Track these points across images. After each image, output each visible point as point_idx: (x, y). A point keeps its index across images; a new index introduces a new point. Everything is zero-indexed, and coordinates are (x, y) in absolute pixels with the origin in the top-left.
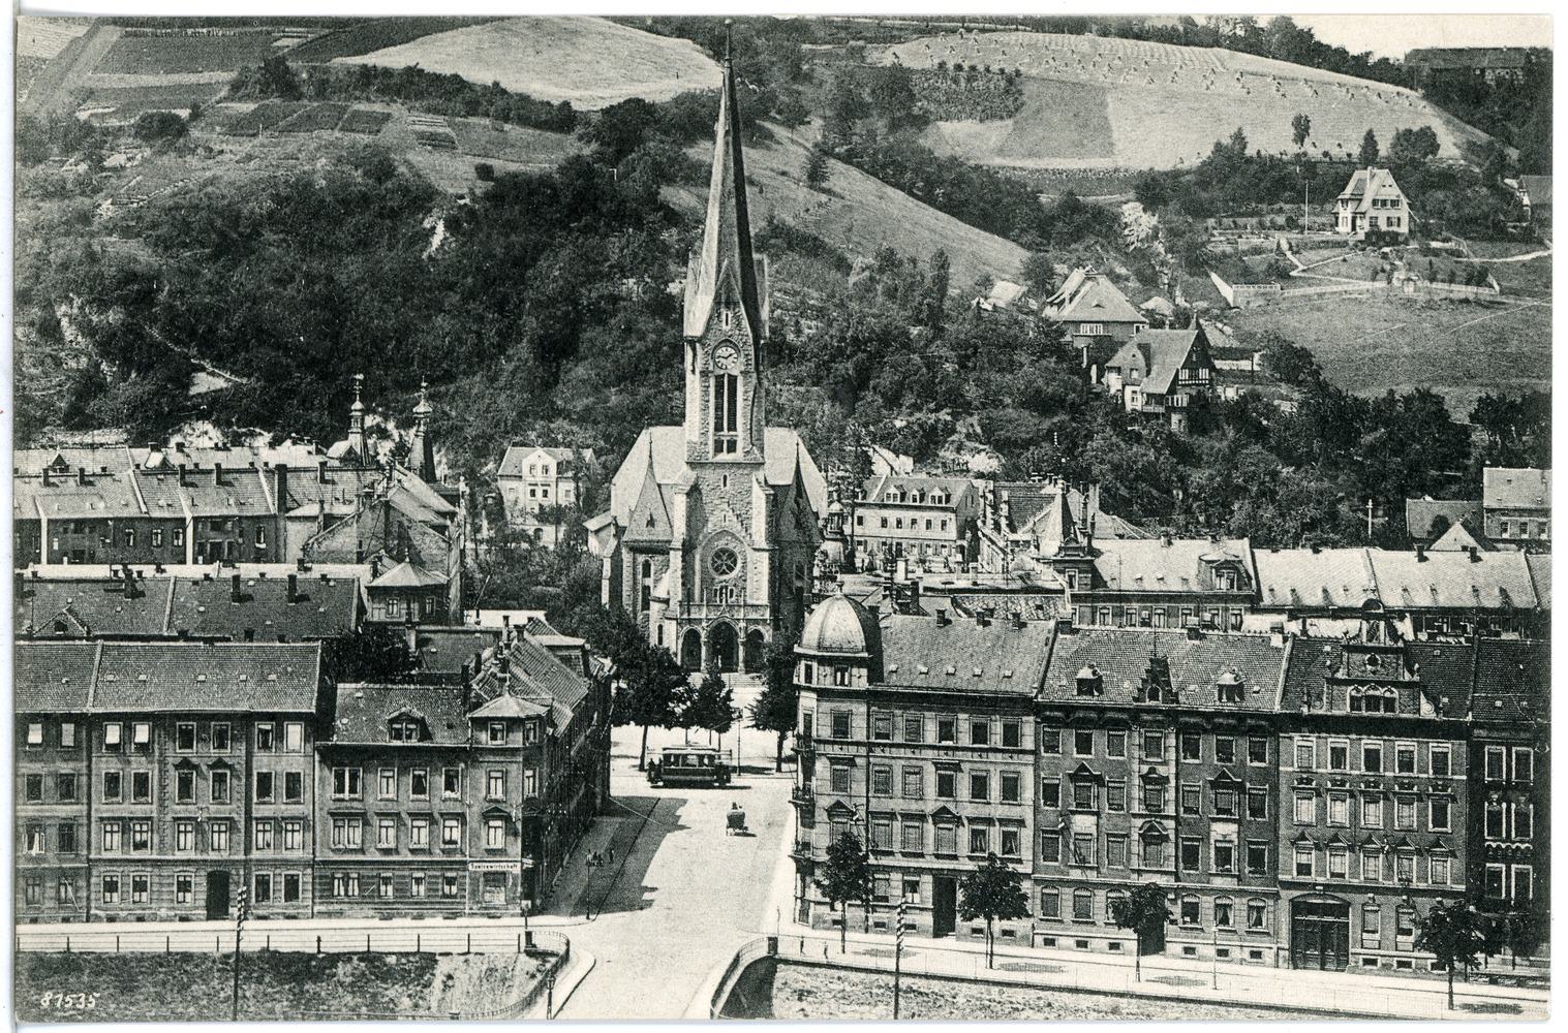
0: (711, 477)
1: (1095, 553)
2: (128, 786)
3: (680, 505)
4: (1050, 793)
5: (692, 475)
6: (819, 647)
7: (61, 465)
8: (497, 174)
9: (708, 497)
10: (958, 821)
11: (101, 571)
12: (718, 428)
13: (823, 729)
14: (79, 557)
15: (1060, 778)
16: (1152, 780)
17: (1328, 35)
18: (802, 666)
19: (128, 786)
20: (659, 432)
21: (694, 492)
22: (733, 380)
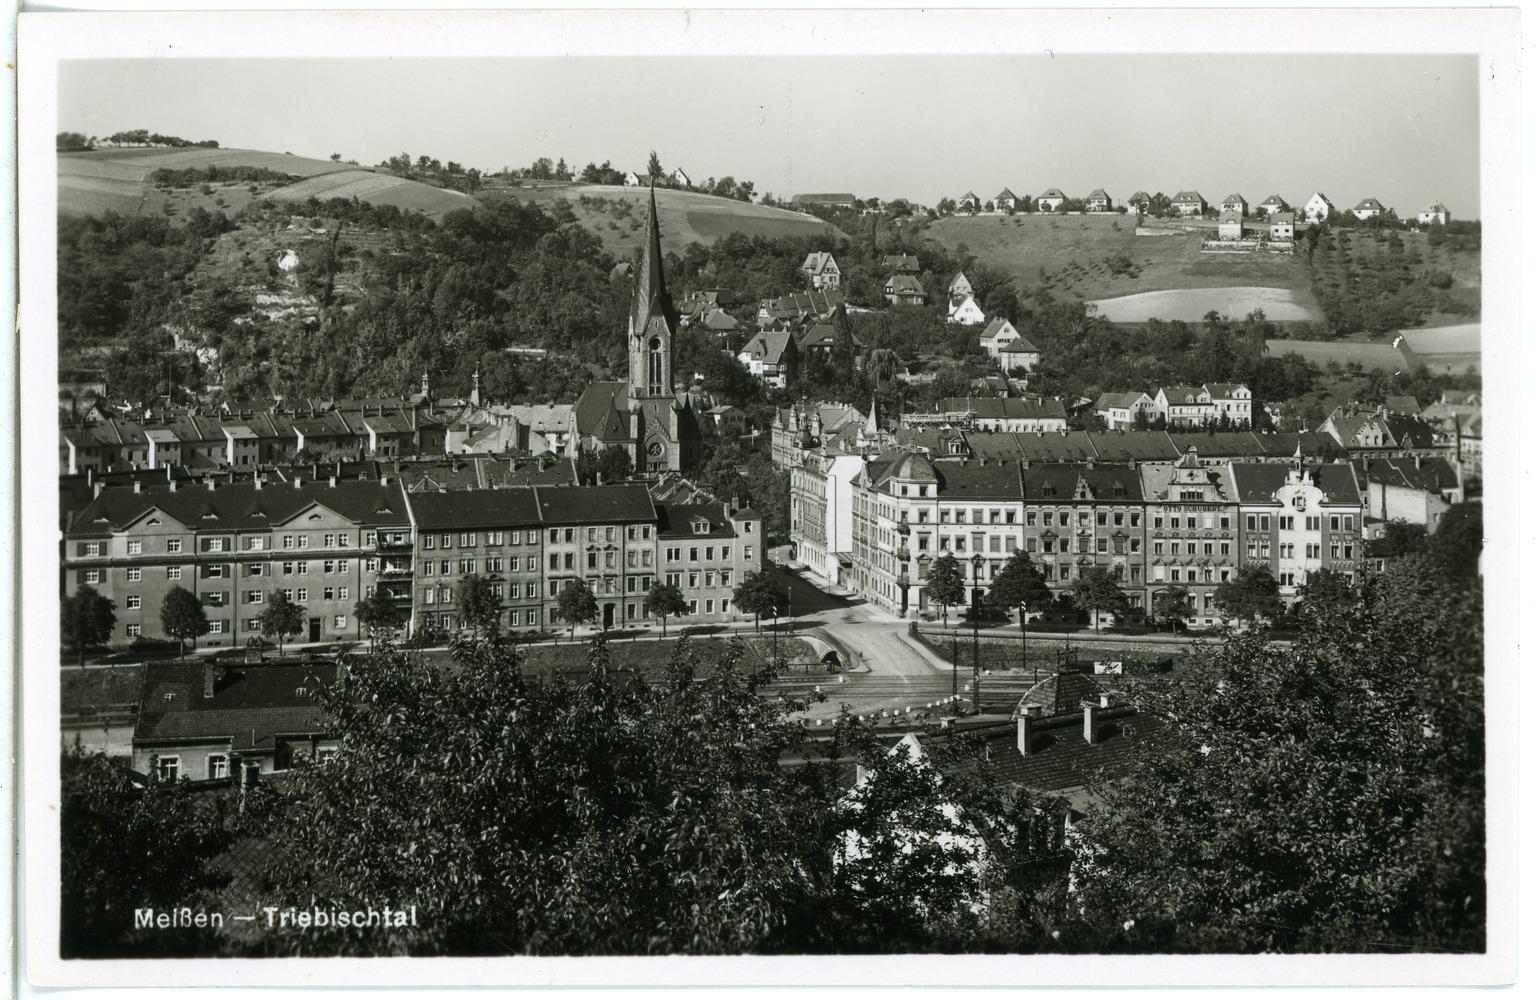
0: (649, 406)
2: (562, 561)
12: (652, 380)
16: (1084, 539)
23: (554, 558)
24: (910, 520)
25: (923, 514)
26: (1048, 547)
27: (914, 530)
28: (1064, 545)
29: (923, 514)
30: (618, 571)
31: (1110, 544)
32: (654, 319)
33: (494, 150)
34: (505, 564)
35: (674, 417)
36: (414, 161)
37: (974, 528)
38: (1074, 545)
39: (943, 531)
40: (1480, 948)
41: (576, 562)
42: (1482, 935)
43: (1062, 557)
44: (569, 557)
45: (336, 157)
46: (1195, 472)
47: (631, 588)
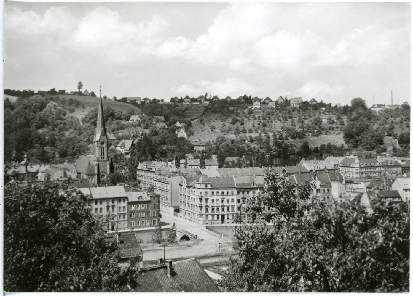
4: (239, 201)
9: (100, 165)
12: (101, 155)
19: (230, 201)
21: (98, 166)
25: (206, 192)
27: (204, 198)
29: (206, 192)
30: (126, 212)
39: (213, 198)
44: (101, 209)
47: (120, 218)
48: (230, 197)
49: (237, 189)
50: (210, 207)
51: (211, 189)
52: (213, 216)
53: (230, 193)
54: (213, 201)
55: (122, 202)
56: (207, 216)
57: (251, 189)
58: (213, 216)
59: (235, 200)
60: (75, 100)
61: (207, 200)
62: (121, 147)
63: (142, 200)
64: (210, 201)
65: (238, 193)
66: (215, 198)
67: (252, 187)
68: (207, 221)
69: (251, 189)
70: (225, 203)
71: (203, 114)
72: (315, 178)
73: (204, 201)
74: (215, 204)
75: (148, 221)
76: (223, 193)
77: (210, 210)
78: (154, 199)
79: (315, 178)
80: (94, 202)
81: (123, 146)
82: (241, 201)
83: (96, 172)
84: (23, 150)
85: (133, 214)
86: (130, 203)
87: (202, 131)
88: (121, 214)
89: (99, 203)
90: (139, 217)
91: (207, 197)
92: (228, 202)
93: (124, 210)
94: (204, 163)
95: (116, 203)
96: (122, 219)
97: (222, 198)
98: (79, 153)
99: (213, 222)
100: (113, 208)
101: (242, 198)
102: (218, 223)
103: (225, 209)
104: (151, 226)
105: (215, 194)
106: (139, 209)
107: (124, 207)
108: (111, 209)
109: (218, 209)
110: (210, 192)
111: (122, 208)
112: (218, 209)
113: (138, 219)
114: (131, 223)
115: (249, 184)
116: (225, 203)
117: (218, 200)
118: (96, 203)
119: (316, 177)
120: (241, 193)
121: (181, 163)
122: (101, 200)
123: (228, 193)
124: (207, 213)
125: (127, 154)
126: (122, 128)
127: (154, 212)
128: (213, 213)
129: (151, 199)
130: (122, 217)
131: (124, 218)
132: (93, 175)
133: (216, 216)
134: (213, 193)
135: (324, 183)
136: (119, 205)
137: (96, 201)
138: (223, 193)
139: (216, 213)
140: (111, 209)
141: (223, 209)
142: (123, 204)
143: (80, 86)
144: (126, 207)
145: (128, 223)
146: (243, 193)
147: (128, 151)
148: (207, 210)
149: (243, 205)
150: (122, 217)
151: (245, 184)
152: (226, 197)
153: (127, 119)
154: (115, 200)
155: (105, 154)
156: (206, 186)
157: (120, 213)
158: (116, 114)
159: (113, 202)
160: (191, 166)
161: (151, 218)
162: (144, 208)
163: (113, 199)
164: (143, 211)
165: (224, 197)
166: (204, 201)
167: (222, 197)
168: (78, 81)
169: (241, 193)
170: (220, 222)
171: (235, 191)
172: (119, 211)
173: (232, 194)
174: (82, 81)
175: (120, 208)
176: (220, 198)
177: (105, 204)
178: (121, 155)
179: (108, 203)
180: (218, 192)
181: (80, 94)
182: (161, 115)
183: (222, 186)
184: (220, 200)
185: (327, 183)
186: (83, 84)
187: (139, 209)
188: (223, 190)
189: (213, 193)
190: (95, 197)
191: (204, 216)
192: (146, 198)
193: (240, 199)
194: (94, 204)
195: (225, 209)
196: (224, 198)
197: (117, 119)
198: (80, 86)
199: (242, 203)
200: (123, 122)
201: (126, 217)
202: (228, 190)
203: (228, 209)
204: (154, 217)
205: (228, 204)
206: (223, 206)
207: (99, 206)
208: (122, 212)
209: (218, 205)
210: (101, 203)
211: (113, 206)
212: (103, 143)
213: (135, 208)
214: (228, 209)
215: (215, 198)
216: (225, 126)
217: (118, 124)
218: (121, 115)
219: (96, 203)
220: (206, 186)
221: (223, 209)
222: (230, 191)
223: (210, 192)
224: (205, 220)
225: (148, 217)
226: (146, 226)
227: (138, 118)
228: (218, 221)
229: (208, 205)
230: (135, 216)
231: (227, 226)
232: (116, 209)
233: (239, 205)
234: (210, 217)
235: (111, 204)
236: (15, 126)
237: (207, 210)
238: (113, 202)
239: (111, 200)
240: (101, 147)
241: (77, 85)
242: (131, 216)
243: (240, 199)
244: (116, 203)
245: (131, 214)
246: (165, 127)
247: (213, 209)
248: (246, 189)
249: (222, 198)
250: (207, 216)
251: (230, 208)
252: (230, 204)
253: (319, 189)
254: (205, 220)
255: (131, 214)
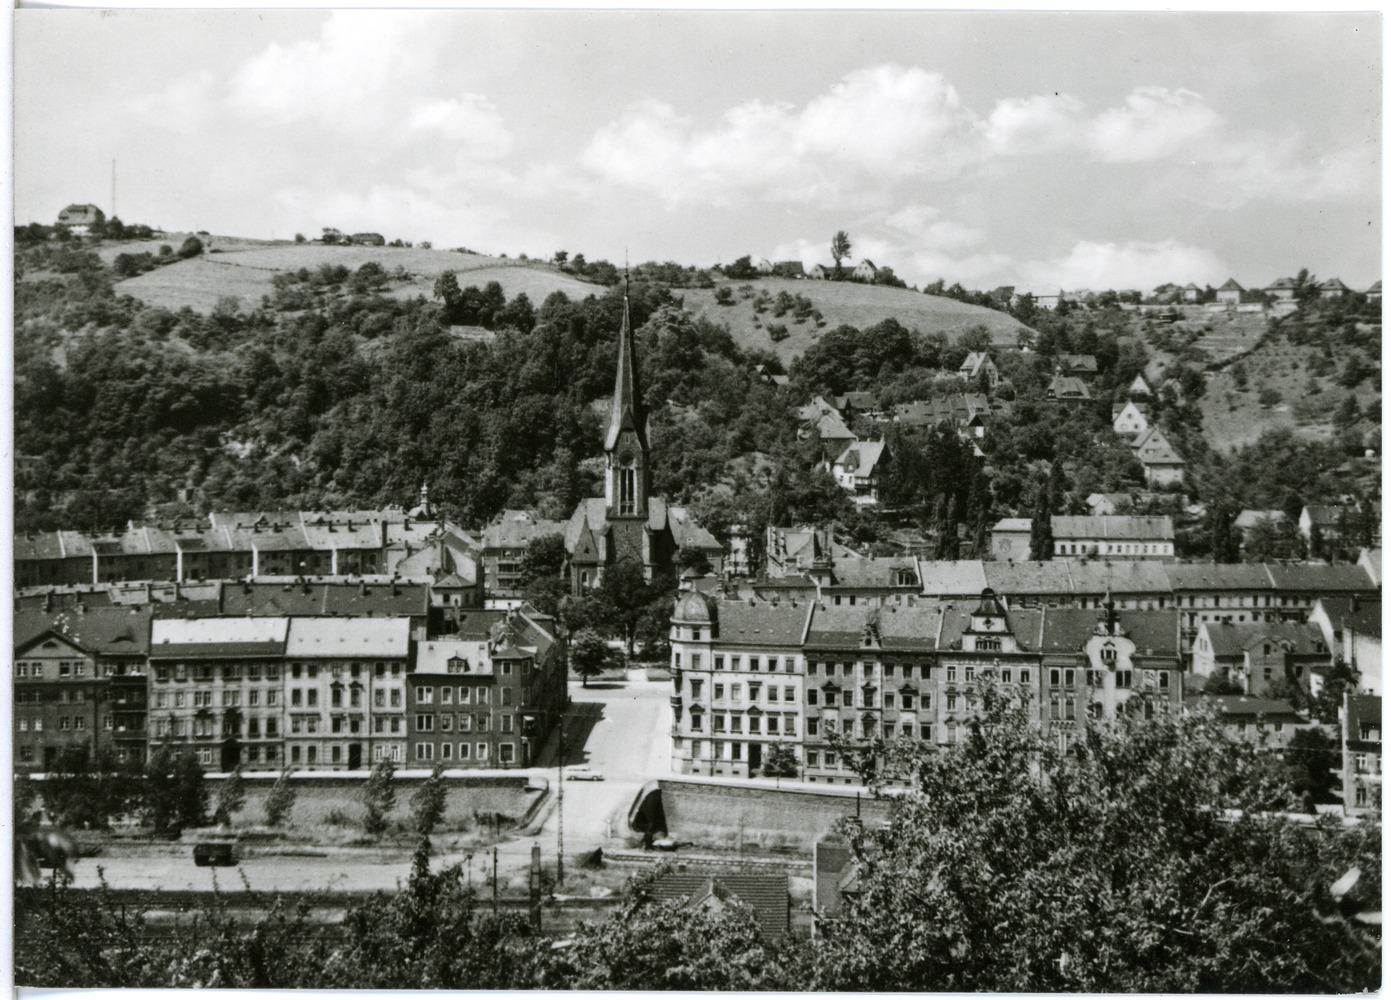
0: (620, 526)
1: (833, 565)
2: (781, 694)
3: (602, 542)
4: (812, 697)
5: (609, 524)
6: (684, 618)
7: (264, 522)
8: (1334, 627)
9: (617, 535)
10: (760, 713)
11: (289, 579)
12: (623, 499)
13: (686, 662)
14: (276, 571)
15: (895, 691)
16: (869, 691)
17: (970, 288)
18: (674, 628)
19: (781, 694)
20: (591, 502)
21: (610, 535)
22: (631, 472)
23: (297, 694)
24: (682, 667)
25: (696, 658)
26: (907, 703)
27: (687, 677)
28: (926, 701)
29: (696, 658)
30: (403, 708)
31: (899, 699)
32: (625, 435)
33: (627, 250)
34: (244, 700)
35: (646, 539)
36: (571, 258)
37: (751, 677)
38: (859, 698)
39: (718, 678)
40: (21, 979)
41: (320, 698)
42: (68, 977)
43: (925, 715)
44: (313, 693)
45: (504, 256)
46: (992, 620)
47: (379, 729)
48: (781, 681)
49: (805, 652)
50: (708, 711)
51: (712, 646)
52: (718, 744)
53: (781, 665)
54: (719, 690)
55: (388, 674)
56: (696, 743)
57: (859, 655)
58: (718, 744)
59: (800, 695)
60: (798, 298)
61: (696, 685)
62: (845, 466)
63: (462, 671)
64: (707, 690)
65: (812, 668)
66: (726, 679)
67: (863, 647)
68: (697, 764)
69: (859, 655)
70: (763, 702)
71: (1259, 346)
72: (1111, 629)
73: (687, 687)
74: (726, 702)
75: (482, 747)
76: (754, 664)
77: (706, 722)
78: (507, 670)
79: (1111, 629)
80: (289, 666)
81: (854, 462)
82: (821, 696)
83: (603, 555)
84: (521, 469)
85: (429, 719)
86: (417, 681)
87: (1233, 409)
88: (385, 715)
89: (305, 675)
90: (450, 729)
91: (699, 676)
92: (773, 697)
93: (394, 703)
94: (1049, 531)
95: (364, 677)
96: (387, 732)
97: (751, 683)
98: (693, 482)
99: (718, 766)
100: (355, 694)
101: (902, 691)
102: (736, 773)
103: (764, 721)
104: (495, 765)
105: (727, 663)
106: (449, 701)
107: (395, 693)
108: (346, 696)
109: (736, 721)
110: (707, 657)
111: (388, 695)
112: (736, 721)
113: (446, 736)
114: (421, 747)
115: (856, 637)
116: (763, 702)
117: (735, 687)
118: (297, 674)
119: (1117, 626)
120: (821, 668)
121: (1055, 533)
122: (315, 664)
123: (772, 664)
124: (696, 735)
125: (862, 490)
126: (922, 395)
127: (507, 718)
128: (719, 735)
129: (494, 670)
130: (387, 725)
131: (395, 729)
132: (594, 565)
133: (728, 749)
134: (719, 662)
135: (1149, 652)
136: (377, 684)
137: (298, 665)
138: (754, 664)
139: (728, 735)
140: (346, 696)
141: (754, 725)
142: (391, 682)
143: (842, 245)
144: (403, 693)
145: (411, 746)
146: (830, 670)
147: (866, 482)
148: (696, 722)
149: (830, 714)
150: (387, 725)
151: (845, 634)
152: (768, 680)
153: (955, 363)
154: (363, 666)
155: (635, 494)
156: (697, 636)
157: (381, 710)
158: (920, 346)
159: (356, 672)
160: (1073, 539)
161: (493, 738)
162: (467, 701)
163: (356, 663)
164: (464, 710)
165: (758, 678)
166: (687, 687)
167: (751, 677)
168: (835, 234)
169: (821, 668)
170: (744, 767)
171: (800, 661)
172: (378, 704)
173: (790, 670)
174: (845, 229)
175: (380, 693)
176: (743, 680)
177: (323, 681)
178: (842, 493)
179: (336, 676)
180: (736, 660)
181: (840, 274)
182: (1088, 352)
183: (754, 639)
184: (745, 690)
185: (1165, 653)
186: (850, 239)
187: (449, 701)
188: (755, 654)
189: (719, 662)
190: (294, 650)
191: (687, 744)
192: (481, 665)
193: (818, 689)
194: (289, 675)
195: (764, 721)
196: (759, 683)
197: (920, 362)
198: (842, 245)
199: (824, 704)
200: (940, 376)
201: (403, 725)
202: (772, 655)
203: (773, 725)
204: (507, 732)
205: (772, 707)
206: (753, 711)
207: (305, 683)
208: (388, 708)
209: (735, 708)
210: (313, 673)
211: (356, 687)
212: (626, 459)
213: (436, 698)
214: (773, 725)
215: (726, 679)
216: (1317, 391)
217: (911, 380)
218: (940, 350)
219: (297, 674)
220: (697, 636)
221: (754, 725)
222: (781, 659)
223: (707, 657)
224: (689, 756)
225: (481, 732)
226: (474, 764)
227: (985, 361)
228: (737, 766)
229: (701, 704)
230: (436, 728)
231: (729, 788)
232: (364, 697)
233: (812, 711)
234: (707, 750)
235: (347, 678)
236: (512, 388)
237: (696, 722)
238: (356, 672)
239: (347, 666)
240: (623, 473)
241: (829, 245)
242: (421, 726)
243: (818, 689)
244: (364, 677)
245: (421, 719)
246: (1080, 394)
247: (719, 722)
248: (840, 653)
249: (751, 683)
250: (696, 743)
251: (781, 721)
252: (781, 705)
253: (1128, 674)
254: (689, 756)
255: (421, 719)
